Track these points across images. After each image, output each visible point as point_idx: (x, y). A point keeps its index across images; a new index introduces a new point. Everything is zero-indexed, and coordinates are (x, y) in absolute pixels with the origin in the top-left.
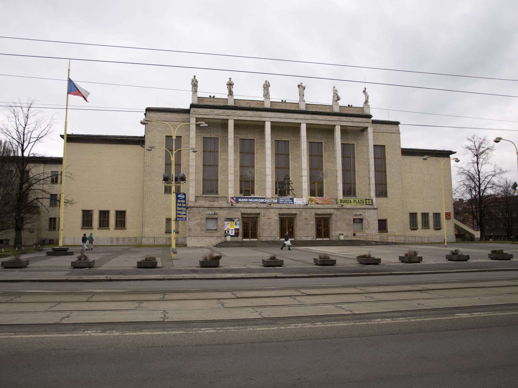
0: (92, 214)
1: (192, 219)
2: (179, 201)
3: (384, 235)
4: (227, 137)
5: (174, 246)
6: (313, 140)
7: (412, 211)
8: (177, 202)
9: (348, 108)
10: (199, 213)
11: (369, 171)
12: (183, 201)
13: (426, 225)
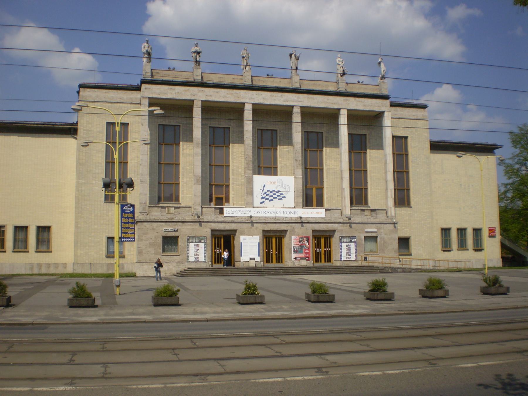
0: (4, 231)
1: (144, 238)
2: (124, 215)
3: (404, 259)
4: (192, 124)
5: (117, 277)
6: (310, 129)
7: (445, 227)
8: (122, 217)
9: (358, 86)
10: (153, 229)
11: (386, 172)
12: (131, 215)
13: (462, 245)
